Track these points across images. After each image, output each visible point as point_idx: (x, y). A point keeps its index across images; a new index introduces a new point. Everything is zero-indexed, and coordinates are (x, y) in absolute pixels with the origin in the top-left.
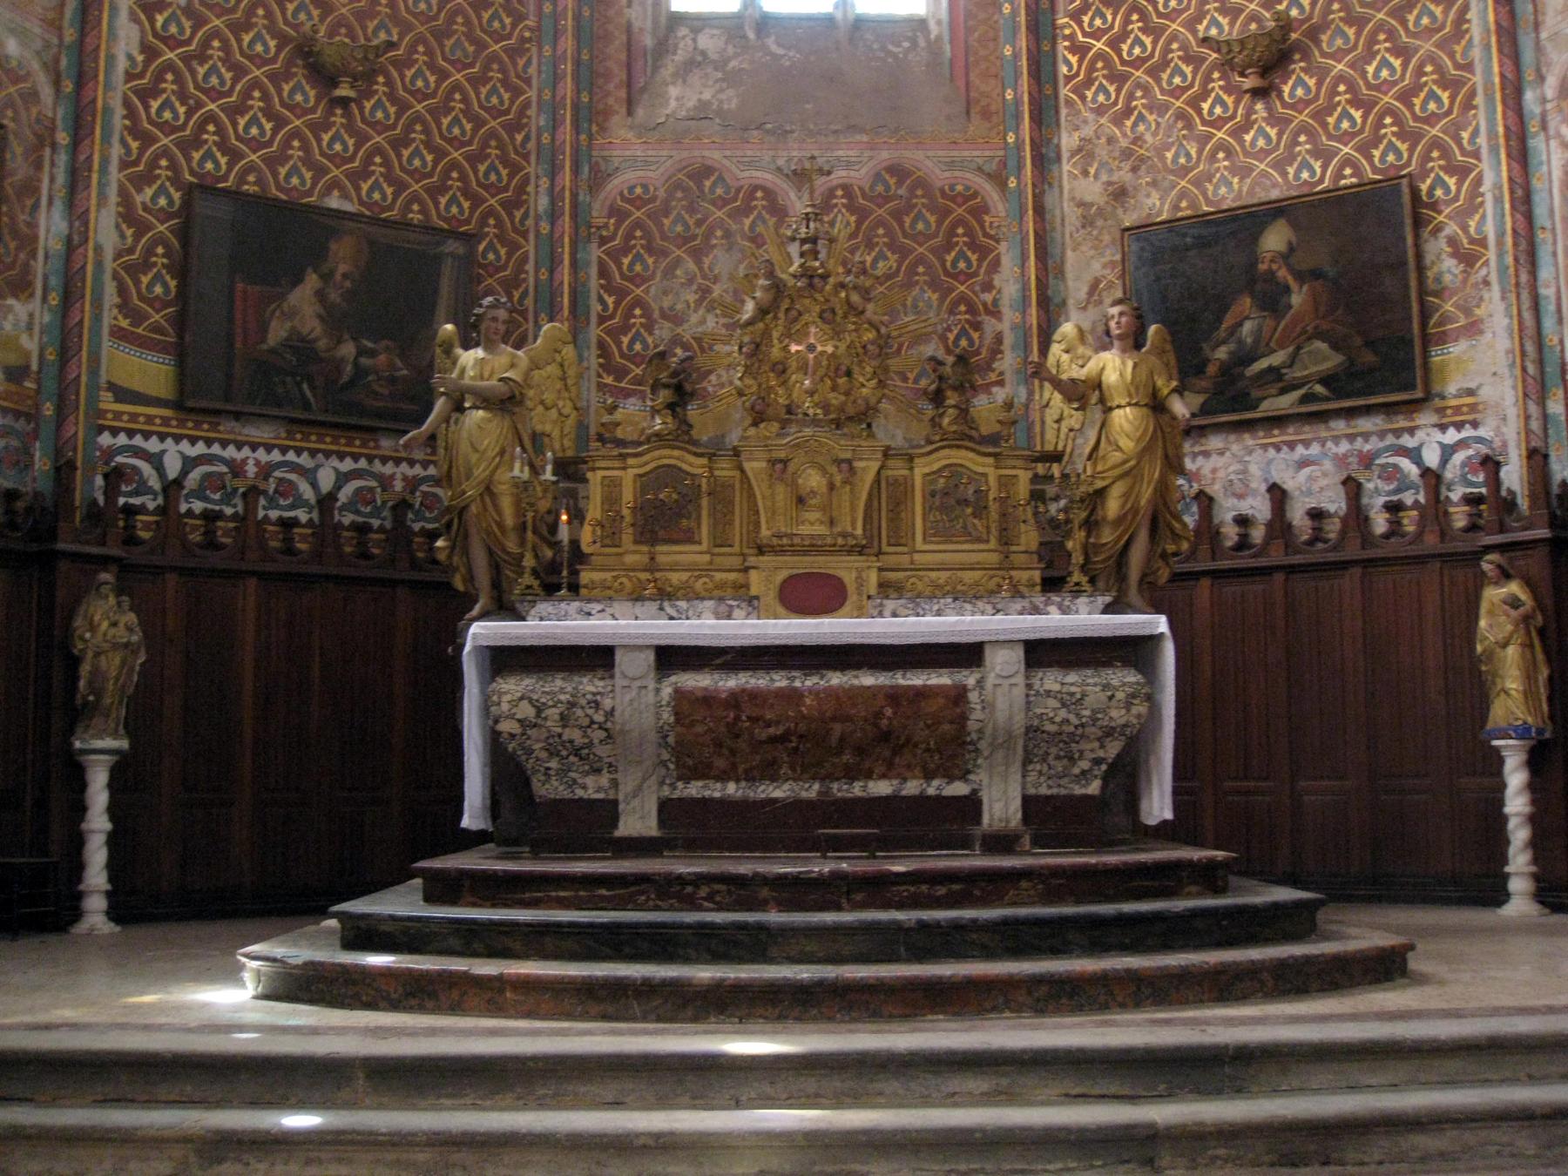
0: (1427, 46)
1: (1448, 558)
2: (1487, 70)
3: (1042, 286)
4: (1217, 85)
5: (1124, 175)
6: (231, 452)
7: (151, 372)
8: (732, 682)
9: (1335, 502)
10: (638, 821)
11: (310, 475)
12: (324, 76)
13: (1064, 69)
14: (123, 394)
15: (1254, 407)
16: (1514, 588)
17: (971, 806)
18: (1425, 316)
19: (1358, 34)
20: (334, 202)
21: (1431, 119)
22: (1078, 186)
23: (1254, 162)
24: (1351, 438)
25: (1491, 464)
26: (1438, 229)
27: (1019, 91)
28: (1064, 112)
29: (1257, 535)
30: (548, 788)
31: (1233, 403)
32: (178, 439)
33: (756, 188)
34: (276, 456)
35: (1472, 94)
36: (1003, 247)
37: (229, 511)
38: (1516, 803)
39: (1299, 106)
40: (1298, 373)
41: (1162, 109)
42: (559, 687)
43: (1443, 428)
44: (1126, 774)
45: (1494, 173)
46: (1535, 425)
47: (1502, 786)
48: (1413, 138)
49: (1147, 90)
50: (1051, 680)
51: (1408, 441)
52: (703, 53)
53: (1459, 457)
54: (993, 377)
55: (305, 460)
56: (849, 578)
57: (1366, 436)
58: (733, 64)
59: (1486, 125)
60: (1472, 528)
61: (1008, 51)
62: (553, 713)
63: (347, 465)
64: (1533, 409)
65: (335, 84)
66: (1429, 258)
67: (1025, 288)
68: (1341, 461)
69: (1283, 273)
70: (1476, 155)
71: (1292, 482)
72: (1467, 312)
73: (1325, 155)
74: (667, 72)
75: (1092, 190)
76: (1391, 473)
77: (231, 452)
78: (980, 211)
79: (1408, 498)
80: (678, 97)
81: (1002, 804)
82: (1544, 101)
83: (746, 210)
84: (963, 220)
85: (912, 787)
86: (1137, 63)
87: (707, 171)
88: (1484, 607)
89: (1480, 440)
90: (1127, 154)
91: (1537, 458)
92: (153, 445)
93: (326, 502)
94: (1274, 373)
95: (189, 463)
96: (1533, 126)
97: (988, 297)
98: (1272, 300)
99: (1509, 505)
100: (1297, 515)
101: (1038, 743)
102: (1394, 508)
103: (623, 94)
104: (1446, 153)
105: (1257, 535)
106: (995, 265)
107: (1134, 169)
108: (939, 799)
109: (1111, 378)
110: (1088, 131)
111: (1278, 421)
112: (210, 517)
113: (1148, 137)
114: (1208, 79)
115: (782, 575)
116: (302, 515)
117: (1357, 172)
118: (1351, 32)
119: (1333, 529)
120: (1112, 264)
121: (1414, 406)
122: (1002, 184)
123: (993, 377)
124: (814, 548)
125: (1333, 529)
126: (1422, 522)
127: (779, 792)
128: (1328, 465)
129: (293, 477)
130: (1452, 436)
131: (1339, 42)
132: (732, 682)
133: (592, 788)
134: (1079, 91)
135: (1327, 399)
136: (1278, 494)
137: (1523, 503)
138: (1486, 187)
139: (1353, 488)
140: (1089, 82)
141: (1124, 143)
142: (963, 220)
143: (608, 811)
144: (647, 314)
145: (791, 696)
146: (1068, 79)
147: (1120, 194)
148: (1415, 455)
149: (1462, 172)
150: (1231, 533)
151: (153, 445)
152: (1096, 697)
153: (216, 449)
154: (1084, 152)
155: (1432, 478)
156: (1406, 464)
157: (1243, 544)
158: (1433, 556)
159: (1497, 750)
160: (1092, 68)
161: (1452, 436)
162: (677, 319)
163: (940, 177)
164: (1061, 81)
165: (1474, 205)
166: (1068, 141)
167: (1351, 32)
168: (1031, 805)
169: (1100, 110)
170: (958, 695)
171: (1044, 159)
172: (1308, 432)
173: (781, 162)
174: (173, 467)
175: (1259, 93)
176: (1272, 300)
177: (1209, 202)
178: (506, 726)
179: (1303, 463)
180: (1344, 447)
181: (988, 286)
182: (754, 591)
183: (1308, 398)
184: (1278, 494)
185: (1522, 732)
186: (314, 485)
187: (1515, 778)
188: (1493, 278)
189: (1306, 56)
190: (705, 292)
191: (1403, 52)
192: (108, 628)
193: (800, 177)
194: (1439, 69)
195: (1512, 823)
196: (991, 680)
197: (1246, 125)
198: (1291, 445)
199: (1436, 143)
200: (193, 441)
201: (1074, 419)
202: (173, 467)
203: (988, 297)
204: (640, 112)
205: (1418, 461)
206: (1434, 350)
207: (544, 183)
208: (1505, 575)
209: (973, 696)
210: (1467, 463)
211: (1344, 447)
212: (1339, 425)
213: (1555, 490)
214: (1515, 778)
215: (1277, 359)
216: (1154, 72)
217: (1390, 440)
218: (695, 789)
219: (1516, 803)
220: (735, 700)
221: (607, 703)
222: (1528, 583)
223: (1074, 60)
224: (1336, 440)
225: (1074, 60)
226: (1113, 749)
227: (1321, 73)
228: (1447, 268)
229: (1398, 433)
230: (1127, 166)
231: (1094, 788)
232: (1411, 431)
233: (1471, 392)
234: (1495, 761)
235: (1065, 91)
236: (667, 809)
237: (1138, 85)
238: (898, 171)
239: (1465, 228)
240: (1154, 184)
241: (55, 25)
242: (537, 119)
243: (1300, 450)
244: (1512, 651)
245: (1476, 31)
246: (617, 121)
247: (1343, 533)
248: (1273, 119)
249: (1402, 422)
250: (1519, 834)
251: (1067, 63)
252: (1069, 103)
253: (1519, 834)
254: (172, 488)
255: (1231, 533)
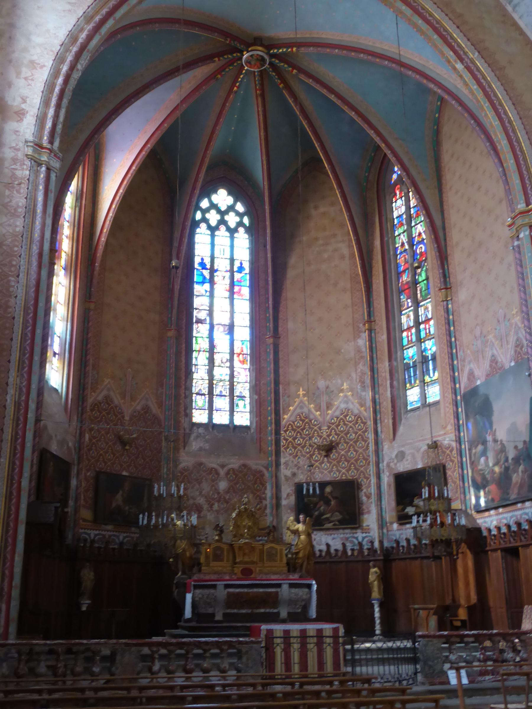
0: (361, 451)
1: (363, 561)
2: (372, 458)
3: (277, 494)
4: (316, 452)
5: (295, 470)
6: (103, 533)
7: (86, 514)
8: (238, 590)
9: (340, 547)
10: (219, 617)
11: (118, 537)
12: (124, 443)
13: (282, 444)
14: (85, 520)
15: (323, 525)
16: (376, 569)
17: (278, 614)
18: (359, 510)
19: (347, 446)
20: (125, 473)
21: (362, 466)
22: (285, 472)
23: (326, 472)
24: (344, 534)
25: (372, 543)
26: (362, 490)
27: (272, 448)
28: (282, 454)
29: (324, 554)
30: (202, 611)
31: (318, 524)
32: (94, 530)
33: (212, 468)
34: (112, 533)
35: (369, 462)
36: (267, 484)
37: (103, 546)
38: (377, 615)
39: (334, 460)
40: (332, 519)
41: (304, 456)
42: (206, 591)
43: (363, 533)
44: (306, 607)
45: (373, 480)
46: (381, 534)
47: (374, 611)
48: (358, 470)
49: (301, 452)
50: (293, 590)
51: (356, 535)
52: (200, 434)
53: (366, 540)
54: (265, 514)
55: (117, 534)
56: (253, 569)
57: (347, 533)
58: (207, 437)
59: (372, 469)
60: (368, 555)
61: (270, 438)
62: (205, 596)
63: (125, 535)
64: (381, 531)
65: (125, 445)
66: (360, 496)
67: (272, 494)
68: (342, 539)
69: (330, 497)
70: (370, 475)
71: (331, 543)
72: (368, 508)
73: (339, 472)
74: (192, 438)
75: (288, 473)
76: (352, 542)
77: (103, 533)
78: (263, 475)
79: (356, 548)
80: (195, 445)
81: (284, 614)
82: (383, 466)
83: (210, 473)
84: (258, 478)
85: (268, 610)
86: (299, 445)
87: (201, 464)
88: (370, 573)
89: (370, 536)
90: (296, 465)
91: (381, 542)
92: (89, 532)
93: (121, 544)
94: (327, 519)
95: (96, 535)
96: (381, 472)
97: (264, 496)
98: (327, 502)
99: (376, 551)
100: (332, 550)
101: (291, 602)
102: (353, 550)
103: (183, 444)
104: (364, 474)
105: (324, 554)
106: (266, 489)
107: (298, 469)
108: (272, 612)
109: (300, 529)
110: (287, 459)
111: (328, 529)
112: (99, 548)
113: (301, 462)
114: (314, 451)
115: (241, 569)
116: (116, 547)
117: (346, 476)
118: (345, 445)
119: (340, 554)
120: (292, 490)
121: (356, 528)
122: (268, 470)
123: (265, 514)
124: (246, 563)
125: (340, 554)
126: (358, 553)
127: (244, 611)
128: (339, 539)
129: (114, 538)
130: (364, 535)
131: (343, 447)
132: (238, 590)
133: (210, 611)
134: (286, 449)
135: (338, 525)
136: (328, 546)
137: (379, 552)
138: (372, 482)
139: (344, 545)
140: (288, 448)
141: (295, 463)
142: (258, 478)
143: (213, 615)
144: (187, 497)
145: (248, 593)
146: (283, 446)
147: (294, 475)
148: (357, 538)
149: (367, 478)
150: (318, 553)
151: (89, 532)
152: (301, 594)
153: (100, 532)
154: (286, 464)
155: (360, 544)
156: (355, 540)
157: (320, 556)
158: (360, 560)
159: (373, 603)
160: (288, 445)
161: (364, 535)
162: (194, 499)
163: (254, 467)
164: (281, 447)
165: (369, 486)
166: (283, 460)
167: (345, 445)
168: (289, 613)
169: (290, 454)
170: (277, 593)
171: (278, 465)
172: (334, 532)
173: (219, 462)
174: (92, 536)
175: (327, 456)
176: (327, 502)
177: (314, 479)
178: (197, 599)
179: (333, 539)
180: (342, 536)
181: (264, 493)
182: (235, 572)
183: (334, 525)
184: (328, 546)
185: (378, 600)
186: (119, 539)
187: (377, 609)
188: (373, 502)
189: (336, 449)
190: (201, 493)
191: (355, 451)
192: (88, 575)
193: (223, 466)
194: (363, 456)
195: (376, 619)
196: (283, 591)
197: (323, 462)
198: (331, 534)
199: (362, 472)
200: (96, 530)
201: (292, 536)
202: (92, 536)
203: (264, 496)
204: (186, 448)
205: (357, 540)
206: (361, 516)
207: (165, 466)
208: (374, 567)
209: (280, 593)
210: (367, 541)
211: (342, 536)
212: (341, 531)
213: (385, 548)
214: (377, 609)
215: (328, 516)
216: (303, 447)
217: (351, 535)
218: (229, 611)
219: (377, 615)
220: (239, 594)
221: (215, 594)
222: (379, 568)
223: (285, 442)
224: (341, 534)
225: (285, 442)
226: (303, 603)
227: (339, 453)
228: (364, 499)
229: (353, 533)
230: (296, 468)
231: (300, 610)
232: (356, 533)
233: (368, 526)
234: (372, 606)
235: (282, 449)
236: (225, 615)
237: (299, 450)
238: (244, 465)
239: (367, 490)
240: (302, 473)
241: (75, 437)
242: (164, 450)
243: (333, 536)
244: (376, 583)
245: (371, 449)
246: (182, 450)
247: (342, 554)
248: (328, 462)
249: (354, 531)
250: (378, 621)
251: (283, 442)
252: (283, 452)
253: (378, 621)
254: (93, 542)
255: (318, 553)
